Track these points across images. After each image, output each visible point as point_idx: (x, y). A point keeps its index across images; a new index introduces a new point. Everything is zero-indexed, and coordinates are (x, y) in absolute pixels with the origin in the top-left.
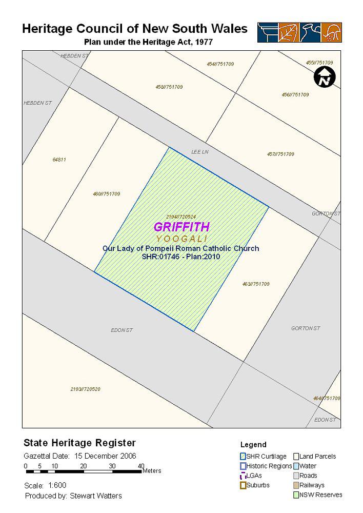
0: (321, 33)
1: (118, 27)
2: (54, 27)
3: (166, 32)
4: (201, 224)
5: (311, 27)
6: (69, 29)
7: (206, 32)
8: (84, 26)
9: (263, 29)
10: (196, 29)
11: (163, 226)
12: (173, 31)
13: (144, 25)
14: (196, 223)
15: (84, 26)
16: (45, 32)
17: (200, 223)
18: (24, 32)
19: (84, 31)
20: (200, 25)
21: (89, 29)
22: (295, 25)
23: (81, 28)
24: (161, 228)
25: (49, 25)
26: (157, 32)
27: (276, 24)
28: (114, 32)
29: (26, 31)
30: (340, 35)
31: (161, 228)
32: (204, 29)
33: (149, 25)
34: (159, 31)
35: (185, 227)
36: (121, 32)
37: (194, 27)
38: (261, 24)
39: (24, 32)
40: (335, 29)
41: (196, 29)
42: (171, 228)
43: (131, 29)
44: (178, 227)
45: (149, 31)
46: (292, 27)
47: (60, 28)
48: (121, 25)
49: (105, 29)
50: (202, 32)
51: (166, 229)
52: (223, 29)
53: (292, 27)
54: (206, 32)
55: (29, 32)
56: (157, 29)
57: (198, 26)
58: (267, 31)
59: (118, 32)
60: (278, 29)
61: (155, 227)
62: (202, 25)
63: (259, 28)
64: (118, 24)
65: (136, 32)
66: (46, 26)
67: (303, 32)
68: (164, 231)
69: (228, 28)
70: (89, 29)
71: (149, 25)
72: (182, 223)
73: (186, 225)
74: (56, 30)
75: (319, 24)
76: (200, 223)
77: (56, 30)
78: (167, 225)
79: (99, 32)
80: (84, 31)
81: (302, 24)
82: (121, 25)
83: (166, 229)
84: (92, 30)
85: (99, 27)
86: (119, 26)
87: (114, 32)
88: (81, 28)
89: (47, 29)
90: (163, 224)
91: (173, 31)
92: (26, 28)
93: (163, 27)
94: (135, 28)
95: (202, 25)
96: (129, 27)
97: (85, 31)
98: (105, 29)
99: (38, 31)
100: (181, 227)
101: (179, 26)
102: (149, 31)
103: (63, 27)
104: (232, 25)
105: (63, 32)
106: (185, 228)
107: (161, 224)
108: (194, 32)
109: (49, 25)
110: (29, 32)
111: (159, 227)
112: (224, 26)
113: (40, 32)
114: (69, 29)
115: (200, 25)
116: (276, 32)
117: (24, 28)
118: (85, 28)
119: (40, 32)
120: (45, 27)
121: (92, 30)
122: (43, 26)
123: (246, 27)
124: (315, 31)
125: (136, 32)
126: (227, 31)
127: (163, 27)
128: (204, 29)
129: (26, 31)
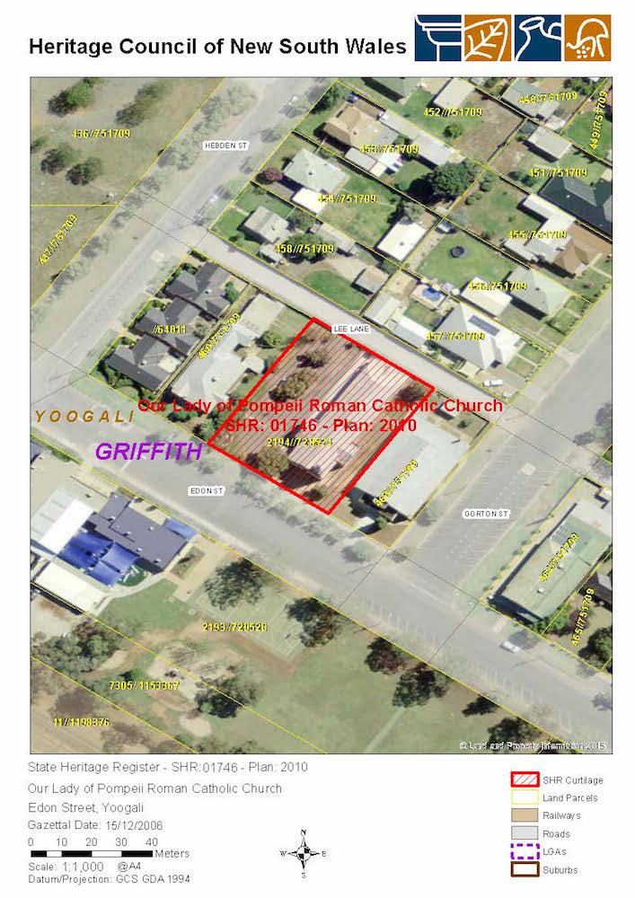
0: (562, 39)
1: (189, 44)
2: (81, 43)
3: (268, 52)
4: (187, 447)
5: (540, 25)
6: (107, 47)
7: (336, 52)
8: (131, 42)
9: (428, 30)
10: (319, 46)
11: (113, 450)
12: (281, 50)
13: (233, 41)
14: (176, 444)
15: (131, 42)
16: (67, 52)
17: (185, 444)
18: (31, 52)
19: (132, 50)
20: (326, 41)
21: (141, 48)
22: (502, 21)
23: (127, 46)
24: (109, 452)
25: (72, 41)
26: (253, 52)
27: (457, 18)
28: (182, 52)
29: (36, 50)
30: (607, 44)
31: (109, 452)
32: (333, 47)
33: (242, 40)
34: (257, 50)
35: (155, 451)
36: (194, 52)
37: (316, 44)
38: (423, 18)
39: (31, 52)
40: (593, 30)
41: (319, 46)
42: (128, 454)
43: (210, 48)
44: (141, 451)
45: (241, 51)
46: (495, 24)
47: (92, 44)
48: (194, 40)
49: (154, 49)
50: (329, 52)
51: (120, 455)
52: (365, 48)
53: (495, 24)
54: (336, 52)
55: (41, 52)
56: (254, 47)
57: (323, 43)
58: (437, 36)
59: (189, 52)
60: (463, 30)
61: (98, 451)
62: (329, 40)
63: (418, 28)
64: (189, 40)
65: (220, 52)
66: (69, 41)
67: (520, 38)
68: (115, 458)
69: (373, 44)
70: (141, 48)
71: (242, 40)
72: (148, 444)
73: (158, 448)
74: (84, 48)
75: (557, 18)
76: (185, 444)
77: (84, 48)
78: (121, 448)
79: (157, 52)
80: (132, 50)
81: (519, 19)
82: (194, 40)
83: (120, 455)
84: (145, 48)
85: (157, 44)
86: (191, 42)
87: (182, 52)
88: (127, 46)
89: (70, 46)
90: (114, 446)
91: (281, 50)
92: (36, 46)
93: (265, 44)
94: (217, 46)
95: (329, 40)
96: (207, 44)
97: (135, 50)
98: (154, 49)
99: (55, 50)
100: (148, 451)
101: (289, 41)
102: (241, 51)
103: (98, 45)
104: (380, 40)
105: (98, 51)
106: (157, 454)
107: (110, 447)
108: (316, 52)
109: (72, 41)
110: (41, 52)
111: (105, 452)
112: (365, 43)
113: (58, 52)
114: (107, 47)
115: (326, 41)
116: (456, 36)
117: (32, 46)
118: (133, 46)
119: (58, 52)
120: (67, 44)
121: (145, 48)
122: (65, 42)
123: (404, 44)
124: (549, 35)
125: (220, 52)
126: (370, 50)
127: (265, 44)
128: (333, 47)
129: (36, 50)
